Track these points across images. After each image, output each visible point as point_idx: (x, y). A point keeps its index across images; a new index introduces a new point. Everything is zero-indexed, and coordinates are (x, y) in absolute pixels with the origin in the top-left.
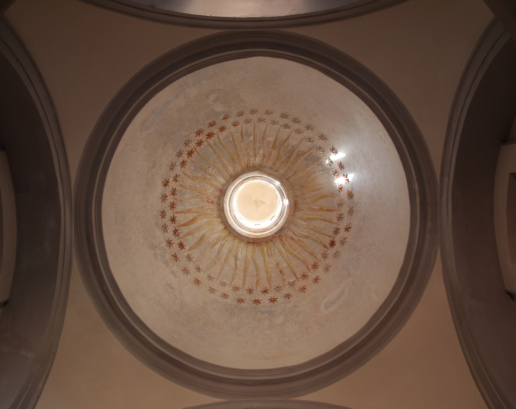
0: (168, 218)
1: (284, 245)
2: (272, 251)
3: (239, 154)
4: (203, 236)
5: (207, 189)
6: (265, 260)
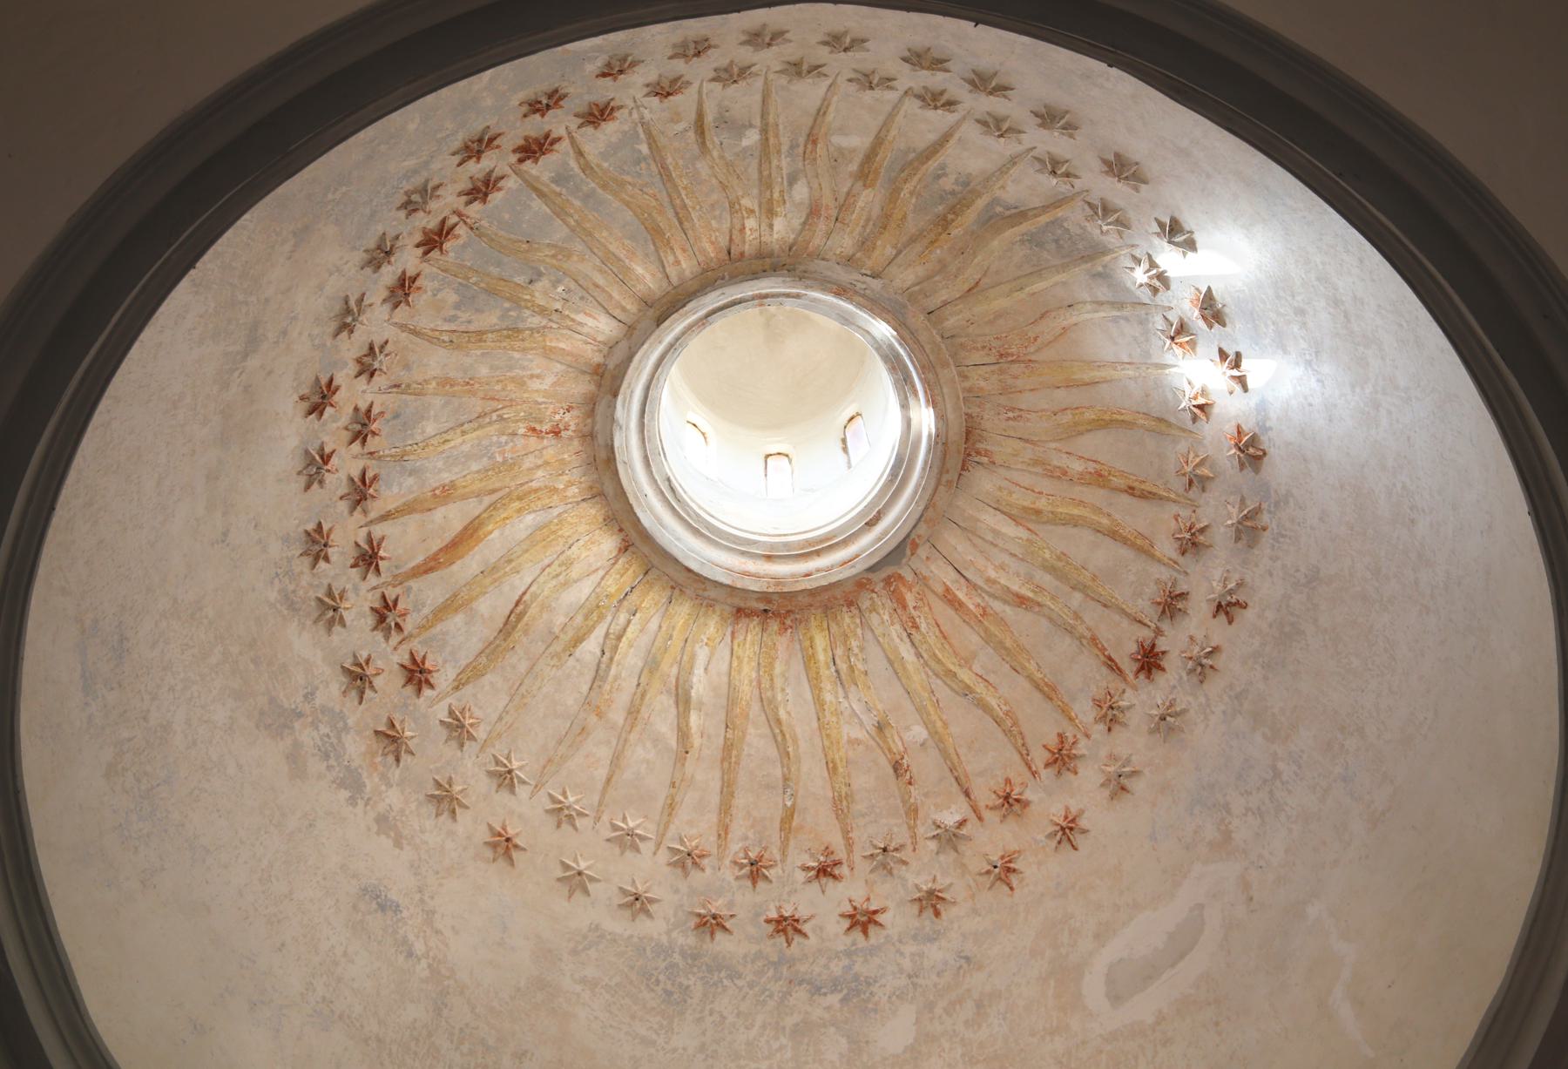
0: (342, 553)
1: (913, 631)
2: (856, 655)
3: (685, 206)
4: (517, 604)
5: (529, 373)
6: (819, 703)
